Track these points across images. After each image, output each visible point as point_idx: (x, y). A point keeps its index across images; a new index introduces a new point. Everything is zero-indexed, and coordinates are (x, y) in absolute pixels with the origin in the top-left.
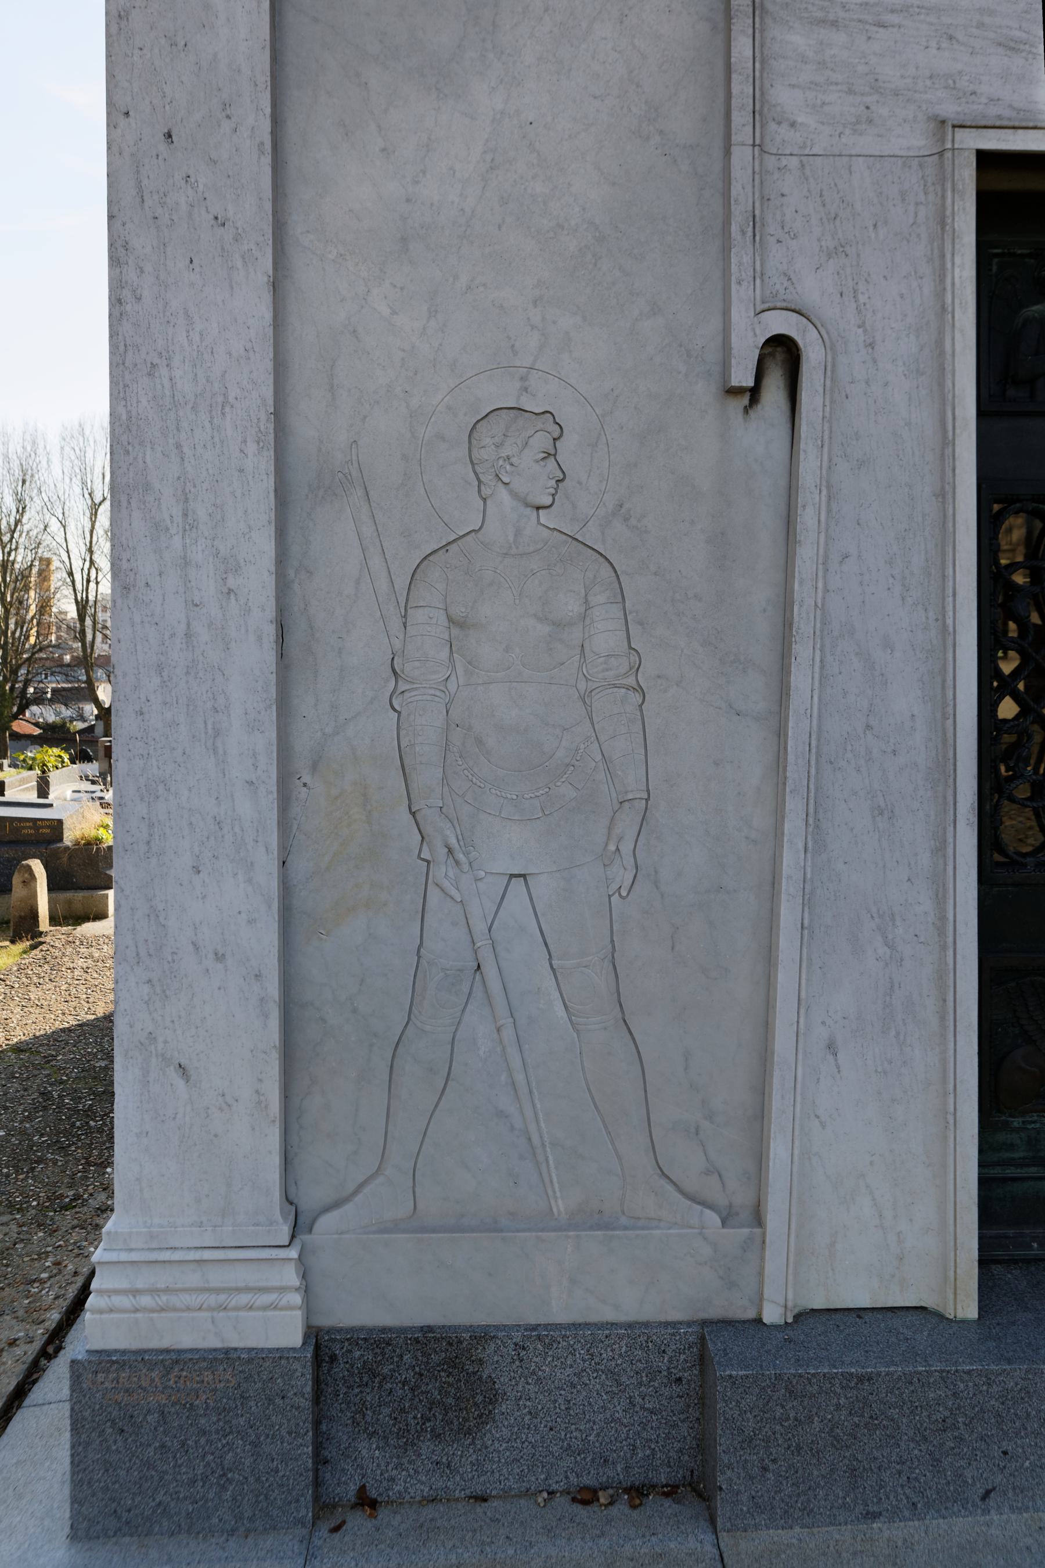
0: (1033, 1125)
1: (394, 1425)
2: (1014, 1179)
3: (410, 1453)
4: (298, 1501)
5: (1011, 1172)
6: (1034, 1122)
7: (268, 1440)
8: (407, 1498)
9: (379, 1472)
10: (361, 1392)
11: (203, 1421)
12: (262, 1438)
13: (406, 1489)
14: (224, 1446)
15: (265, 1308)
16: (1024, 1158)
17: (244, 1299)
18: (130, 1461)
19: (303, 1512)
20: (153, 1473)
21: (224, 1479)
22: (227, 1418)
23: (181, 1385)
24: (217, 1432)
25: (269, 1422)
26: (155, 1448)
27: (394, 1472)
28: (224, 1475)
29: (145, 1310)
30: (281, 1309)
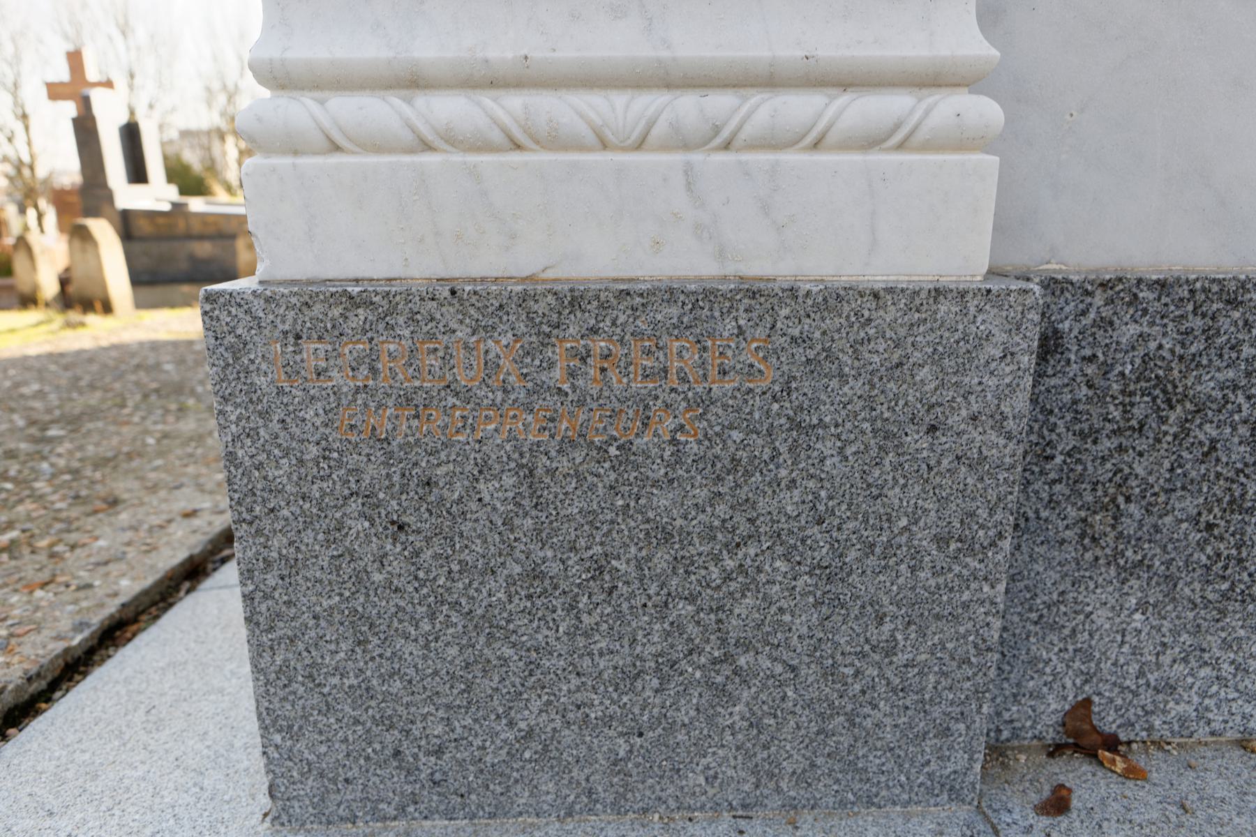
1: (1201, 546)
3: (1233, 621)
4: (946, 732)
7: (871, 561)
8: (1202, 732)
9: (1133, 668)
10: (1121, 449)
11: (663, 500)
12: (852, 555)
13: (1202, 713)
14: (728, 578)
15: (871, 142)
17: (798, 107)
18: (432, 616)
19: (959, 760)
20: (508, 652)
21: (727, 670)
22: (742, 493)
23: (589, 382)
24: (709, 534)
25: (878, 507)
26: (511, 581)
27: (1179, 668)
28: (727, 658)
29: (453, 140)
30: (929, 146)
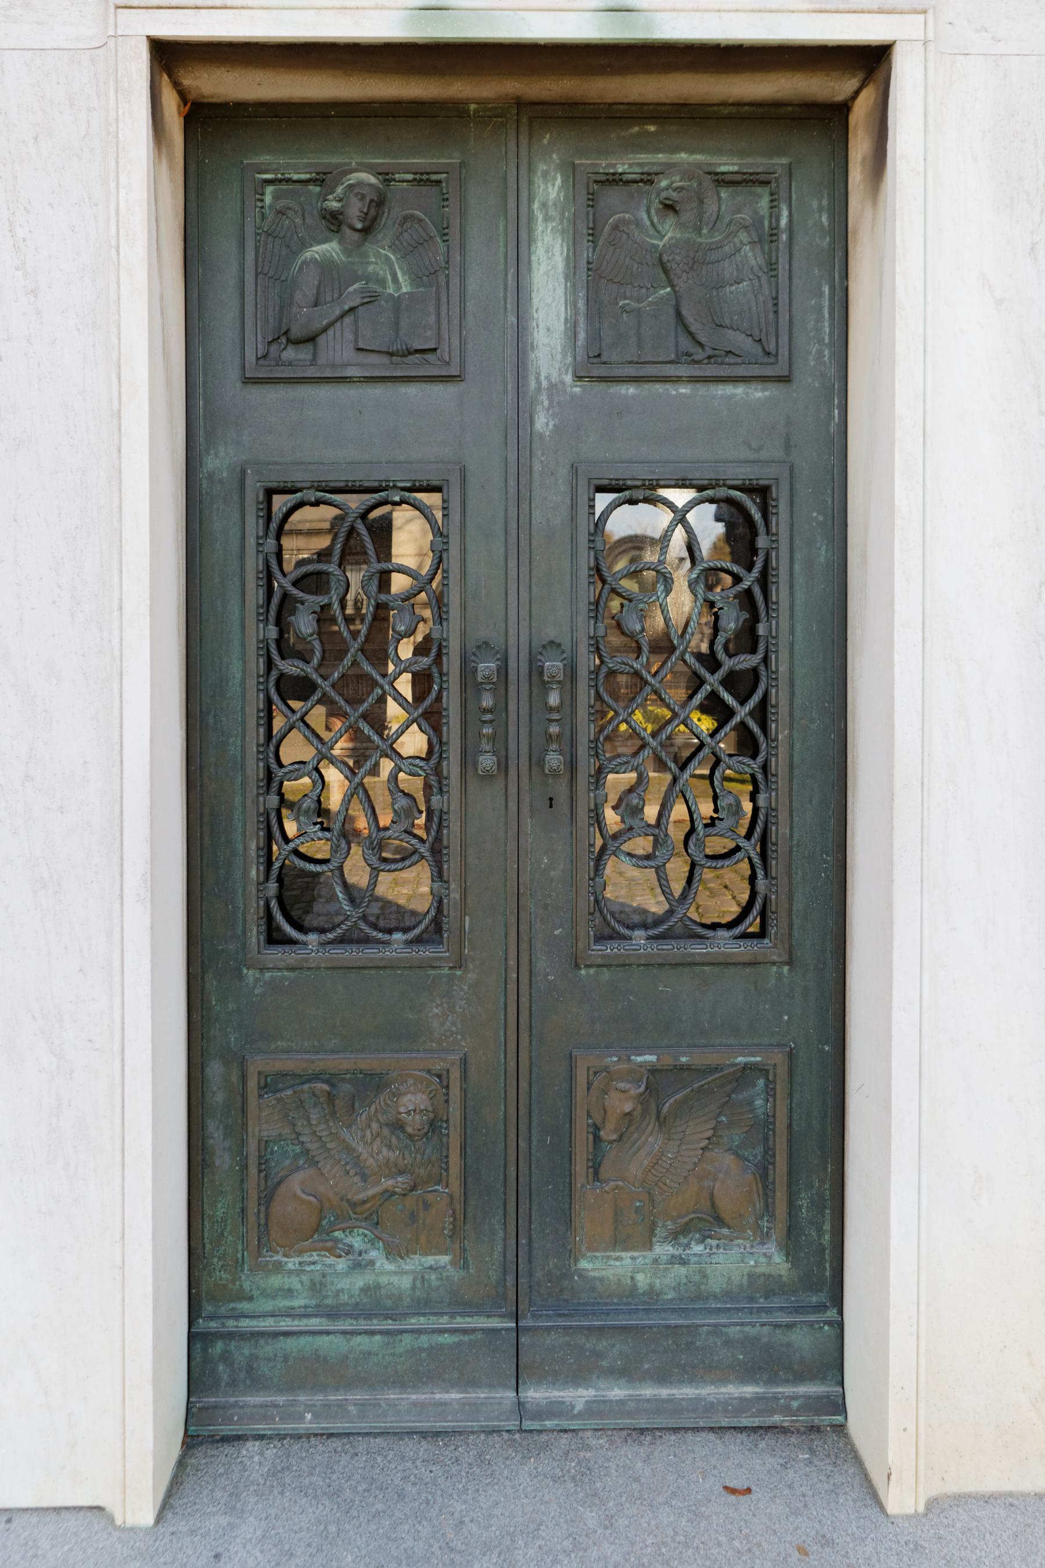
0: (312, 1267)
2: (287, 1334)
5: (286, 1324)
6: (314, 1263)
16: (306, 1307)
